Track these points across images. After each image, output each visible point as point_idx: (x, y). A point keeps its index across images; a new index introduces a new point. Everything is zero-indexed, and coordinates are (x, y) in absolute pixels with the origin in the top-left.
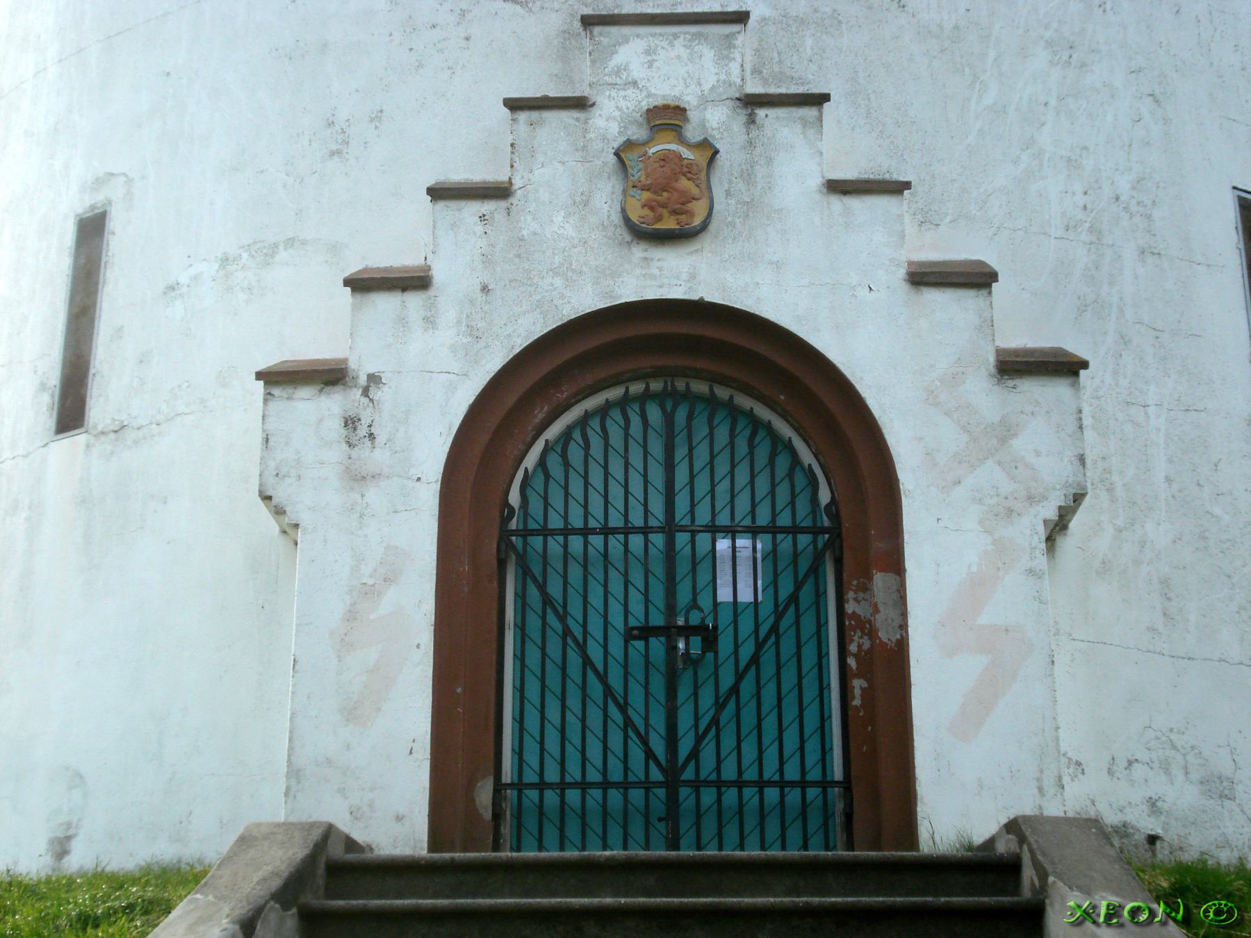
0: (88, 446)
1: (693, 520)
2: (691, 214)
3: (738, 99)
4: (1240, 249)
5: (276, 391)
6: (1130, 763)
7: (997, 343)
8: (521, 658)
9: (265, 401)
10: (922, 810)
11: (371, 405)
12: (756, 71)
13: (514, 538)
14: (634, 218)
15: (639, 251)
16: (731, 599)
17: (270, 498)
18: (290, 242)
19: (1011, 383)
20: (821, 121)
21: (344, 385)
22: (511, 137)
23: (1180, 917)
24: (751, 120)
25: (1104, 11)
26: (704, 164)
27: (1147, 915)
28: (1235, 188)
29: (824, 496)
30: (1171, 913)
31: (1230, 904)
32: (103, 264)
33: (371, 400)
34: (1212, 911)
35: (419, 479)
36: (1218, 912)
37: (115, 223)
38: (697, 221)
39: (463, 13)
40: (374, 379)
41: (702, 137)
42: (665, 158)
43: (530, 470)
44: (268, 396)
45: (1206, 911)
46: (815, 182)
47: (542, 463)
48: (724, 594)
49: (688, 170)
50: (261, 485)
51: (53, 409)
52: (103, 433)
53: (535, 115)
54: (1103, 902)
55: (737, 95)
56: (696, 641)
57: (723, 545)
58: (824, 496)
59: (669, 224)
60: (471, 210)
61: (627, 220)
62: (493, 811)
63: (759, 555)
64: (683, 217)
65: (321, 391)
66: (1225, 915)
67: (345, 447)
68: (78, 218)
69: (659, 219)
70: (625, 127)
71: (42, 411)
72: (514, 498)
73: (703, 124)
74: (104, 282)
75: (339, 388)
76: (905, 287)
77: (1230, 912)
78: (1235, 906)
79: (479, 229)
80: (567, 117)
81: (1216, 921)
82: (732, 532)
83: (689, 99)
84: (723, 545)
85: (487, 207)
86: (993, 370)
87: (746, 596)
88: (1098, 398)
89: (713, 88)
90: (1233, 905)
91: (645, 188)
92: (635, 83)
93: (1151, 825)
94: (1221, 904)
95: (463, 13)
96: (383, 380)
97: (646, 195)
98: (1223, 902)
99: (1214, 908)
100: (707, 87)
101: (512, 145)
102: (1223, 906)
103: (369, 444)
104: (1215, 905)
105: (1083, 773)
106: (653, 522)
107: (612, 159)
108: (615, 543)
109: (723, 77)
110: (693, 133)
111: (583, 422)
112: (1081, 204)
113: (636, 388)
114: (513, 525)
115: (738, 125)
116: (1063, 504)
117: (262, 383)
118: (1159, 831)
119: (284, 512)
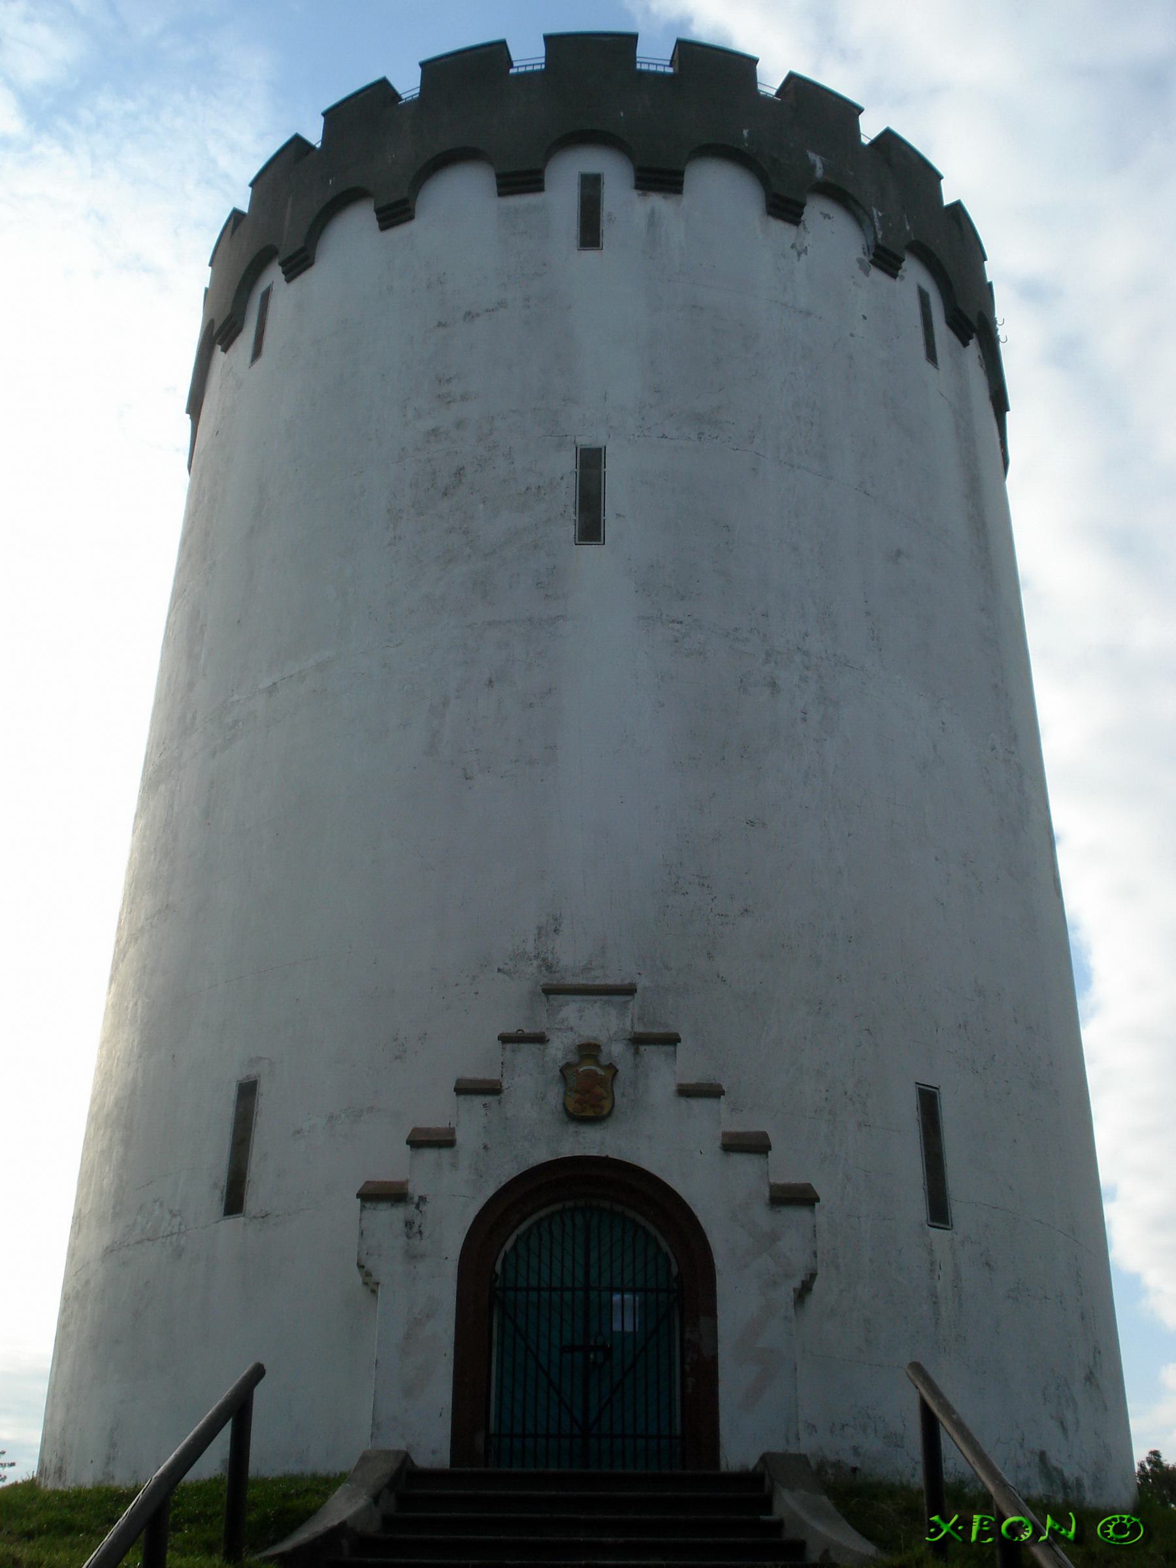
0: (245, 1224)
1: (600, 1282)
3: (629, 1040)
4: (918, 1121)
5: (368, 1205)
7: (772, 1181)
8: (501, 1363)
9: (361, 1210)
10: (722, 1452)
11: (420, 1215)
12: (640, 1019)
13: (498, 1292)
14: (570, 1109)
15: (572, 1128)
16: (620, 1330)
17: (363, 1267)
18: (371, 1109)
19: (778, 1209)
20: (675, 1054)
21: (405, 1202)
22: (502, 1058)
23: (1071, 1534)
24: (637, 1052)
25: (840, 980)
26: (610, 1078)
27: (1030, 1532)
28: (917, 1083)
29: (675, 1270)
30: (1060, 1530)
31: (1134, 1519)
32: (255, 1113)
33: (421, 1212)
34: (1111, 1527)
35: (447, 1258)
36: (1119, 1529)
37: (263, 1088)
38: (605, 1112)
39: (474, 978)
40: (422, 1199)
41: (609, 1062)
42: (590, 1074)
43: (507, 1252)
44: (363, 1208)
45: (1105, 1527)
46: (673, 1088)
47: (515, 1247)
48: (617, 1327)
50: (358, 1259)
51: (222, 1201)
52: (254, 1217)
53: (515, 1045)
54: (975, 1516)
55: (629, 1037)
57: (617, 1298)
58: (675, 1270)
60: (478, 1101)
61: (566, 1110)
63: (637, 1304)
65: (392, 1206)
66: (1128, 1533)
67: (405, 1238)
68: (239, 1083)
70: (566, 1054)
71: (215, 1201)
72: (498, 1267)
73: (610, 1053)
74: (255, 1125)
76: (720, 1152)
77: (1135, 1529)
78: (1140, 1521)
79: (483, 1112)
80: (534, 1048)
81: (1117, 1540)
82: (622, 1291)
83: (602, 1039)
84: (617, 1298)
85: (488, 1099)
86: (768, 1201)
87: (629, 1328)
88: (831, 1213)
89: (615, 1033)
90: (1137, 1520)
91: (576, 1092)
92: (572, 1029)
93: (853, 1461)
94: (1124, 1519)
95: (474, 978)
96: (427, 1200)
98: (1126, 1517)
99: (1114, 1523)
100: (612, 1032)
101: (502, 1063)
102: (1125, 1522)
103: (419, 1237)
104: (1115, 1520)
105: (816, 1432)
106: (577, 1285)
107: (558, 1073)
108: (556, 1297)
109: (621, 1026)
110: (604, 1061)
111: (538, 1223)
113: (570, 1204)
114: (497, 1284)
116: (804, 1279)
117: (359, 1200)
118: (858, 1465)
119: (371, 1275)
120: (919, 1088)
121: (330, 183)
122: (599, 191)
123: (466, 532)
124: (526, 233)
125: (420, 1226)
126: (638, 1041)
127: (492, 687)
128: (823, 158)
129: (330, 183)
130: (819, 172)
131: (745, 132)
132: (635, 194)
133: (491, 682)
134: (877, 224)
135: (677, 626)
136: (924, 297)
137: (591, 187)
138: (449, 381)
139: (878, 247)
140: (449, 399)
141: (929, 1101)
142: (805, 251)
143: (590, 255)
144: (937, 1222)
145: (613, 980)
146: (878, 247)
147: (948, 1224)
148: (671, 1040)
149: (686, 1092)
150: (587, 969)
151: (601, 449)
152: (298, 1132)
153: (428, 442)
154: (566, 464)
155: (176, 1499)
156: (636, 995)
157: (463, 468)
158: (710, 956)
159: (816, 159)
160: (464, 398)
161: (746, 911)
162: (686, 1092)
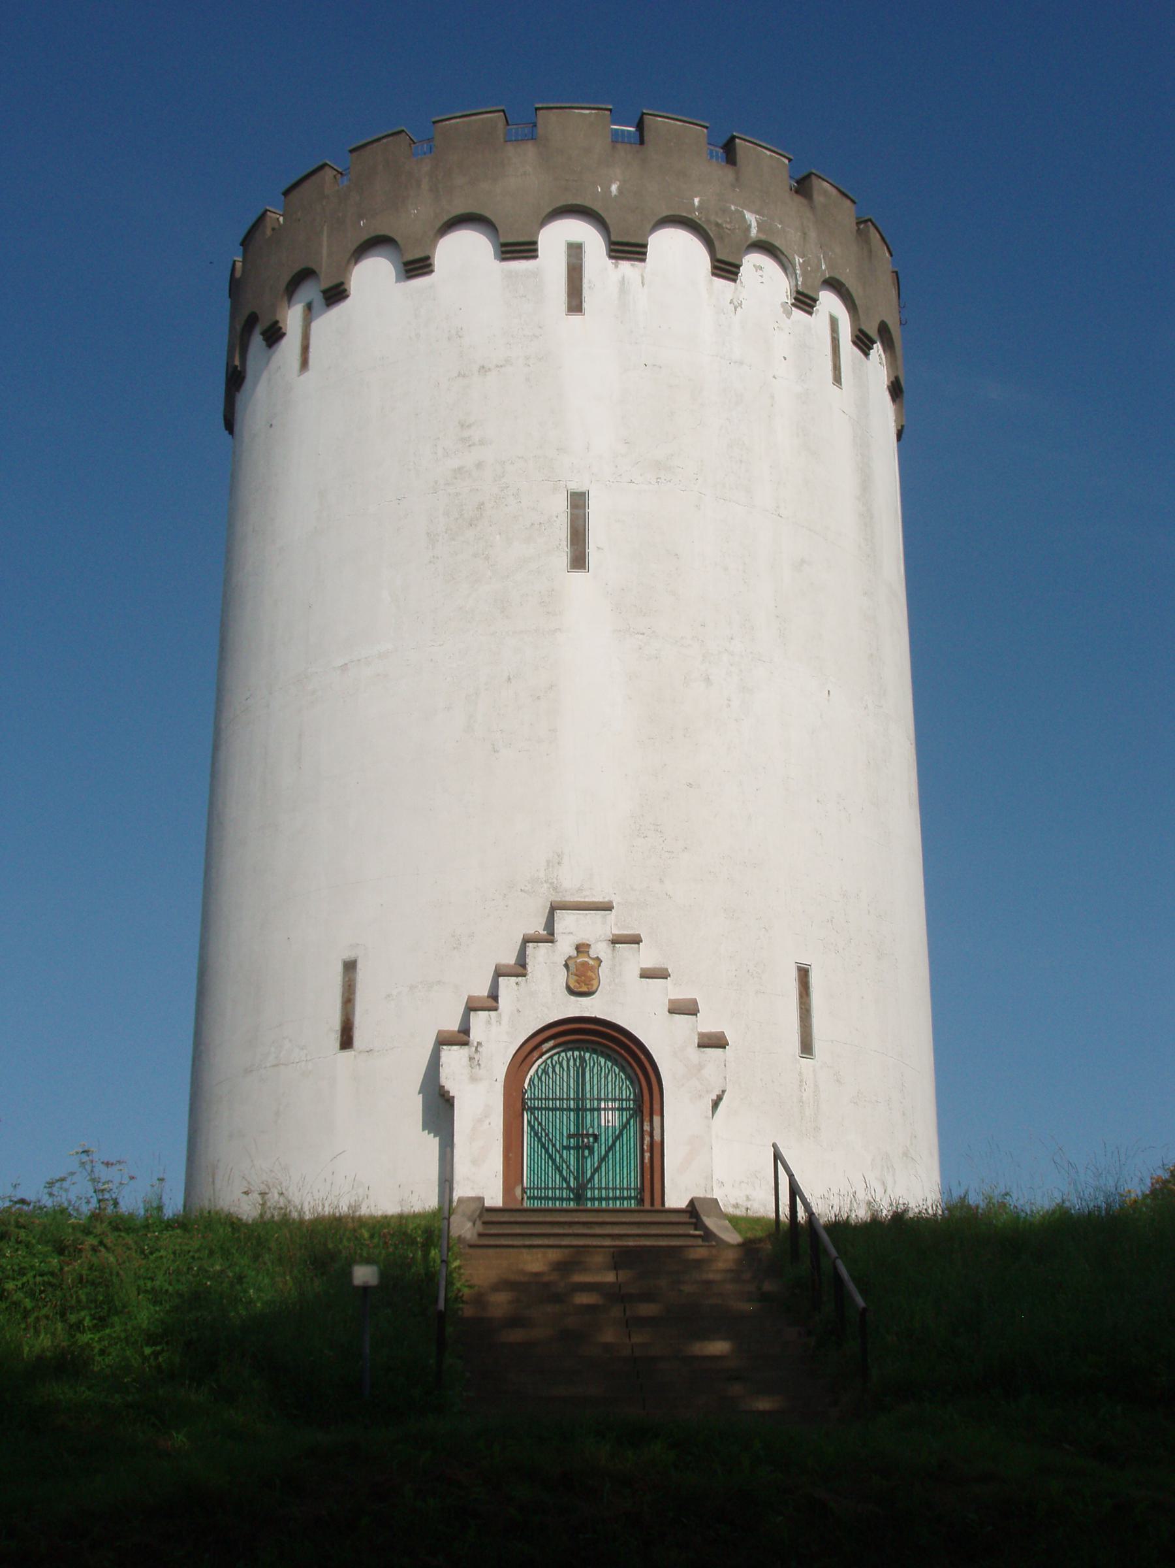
0: (355, 1056)
2: (592, 985)
6: (740, 1183)
7: (699, 1030)
12: (616, 924)
18: (439, 982)
28: (796, 963)
40: (479, 1044)
49: (592, 969)
56: (591, 1139)
59: (584, 989)
62: (787, 1174)
64: (590, 986)
67: (470, 1068)
69: (581, 987)
72: (526, 1086)
75: (467, 1047)
97: (577, 978)
110: (593, 954)
112: (734, 974)
115: (609, 951)
120: (798, 966)
121: (362, 224)
122: (581, 259)
123: (487, 558)
124: (525, 296)
125: (478, 1061)
126: (616, 941)
127: (511, 682)
128: (757, 216)
129: (362, 224)
130: (754, 232)
131: (696, 201)
132: (610, 263)
133: (509, 679)
134: (798, 272)
135: (641, 637)
136: (834, 322)
137: (575, 251)
138: (469, 426)
139: (798, 292)
140: (470, 443)
141: (804, 974)
142: (741, 305)
143: (575, 318)
144: (804, 1054)
145: (598, 898)
146: (798, 292)
147: (812, 1055)
148: (636, 940)
149: (646, 974)
150: (580, 890)
151: (585, 493)
152: (389, 996)
153: (456, 478)
154: (561, 505)
155: (422, 1240)
156: (613, 910)
157: (483, 504)
158: (661, 881)
159: (751, 218)
160: (482, 442)
161: (686, 848)
162: (646, 974)
